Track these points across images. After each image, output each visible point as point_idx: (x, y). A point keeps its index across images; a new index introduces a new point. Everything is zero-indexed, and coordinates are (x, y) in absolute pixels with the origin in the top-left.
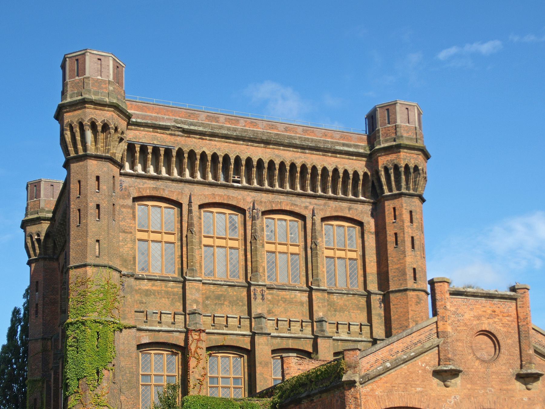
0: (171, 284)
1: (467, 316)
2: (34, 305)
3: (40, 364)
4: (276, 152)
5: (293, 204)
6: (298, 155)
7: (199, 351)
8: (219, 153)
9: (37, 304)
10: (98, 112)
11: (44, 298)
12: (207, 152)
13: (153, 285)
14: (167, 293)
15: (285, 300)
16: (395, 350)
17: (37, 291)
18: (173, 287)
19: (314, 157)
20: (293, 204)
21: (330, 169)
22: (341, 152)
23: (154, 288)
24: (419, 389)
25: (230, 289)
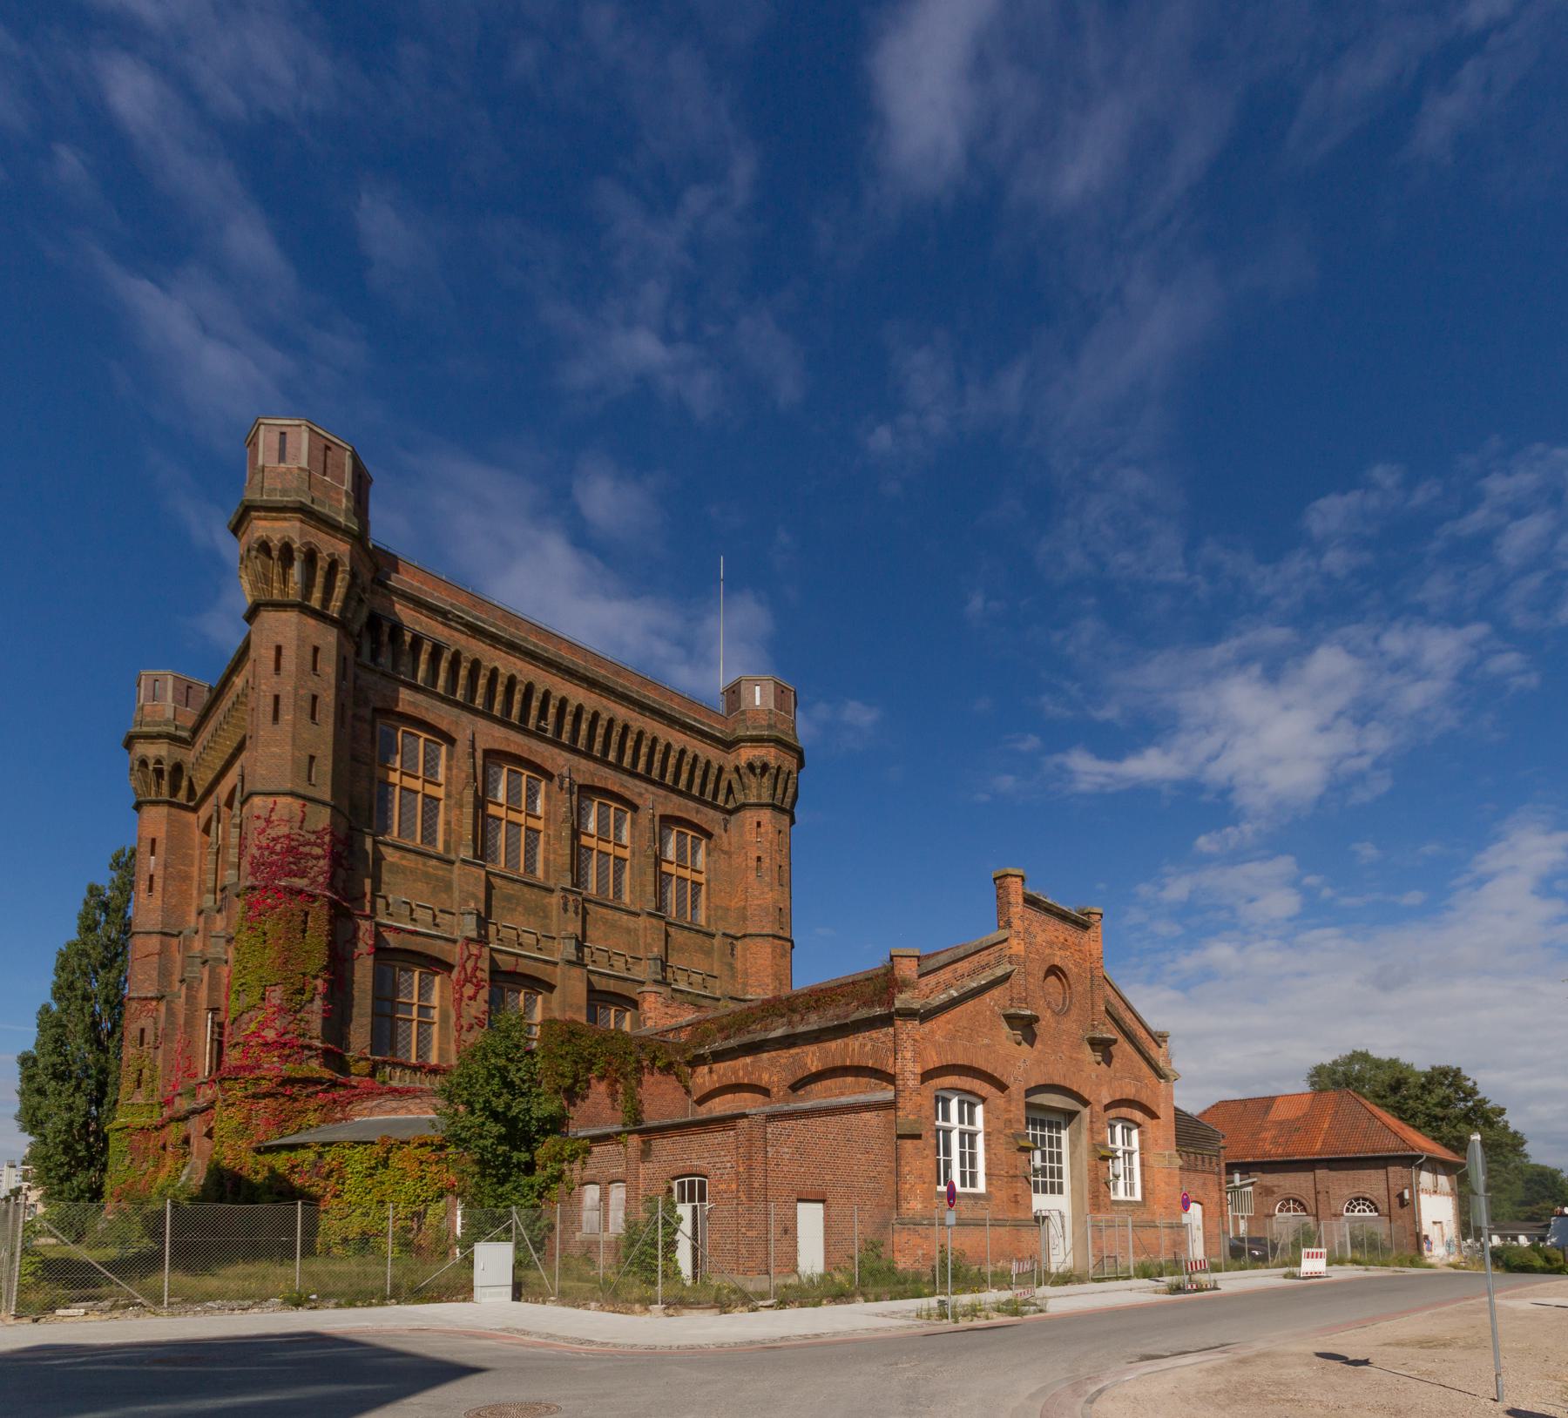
0: (434, 862)
1: (1039, 939)
2: (147, 877)
3: (155, 974)
4: (605, 701)
5: (622, 785)
6: (635, 715)
7: (479, 974)
8: (519, 677)
9: (151, 877)
10: (321, 535)
11: (166, 867)
12: (502, 670)
13: (403, 858)
14: (427, 875)
15: (605, 922)
16: (960, 972)
17: (153, 853)
18: (436, 868)
19: (656, 725)
20: (622, 785)
21: (676, 747)
22: (692, 729)
23: (404, 862)
24: (986, 1041)
25: (526, 889)
